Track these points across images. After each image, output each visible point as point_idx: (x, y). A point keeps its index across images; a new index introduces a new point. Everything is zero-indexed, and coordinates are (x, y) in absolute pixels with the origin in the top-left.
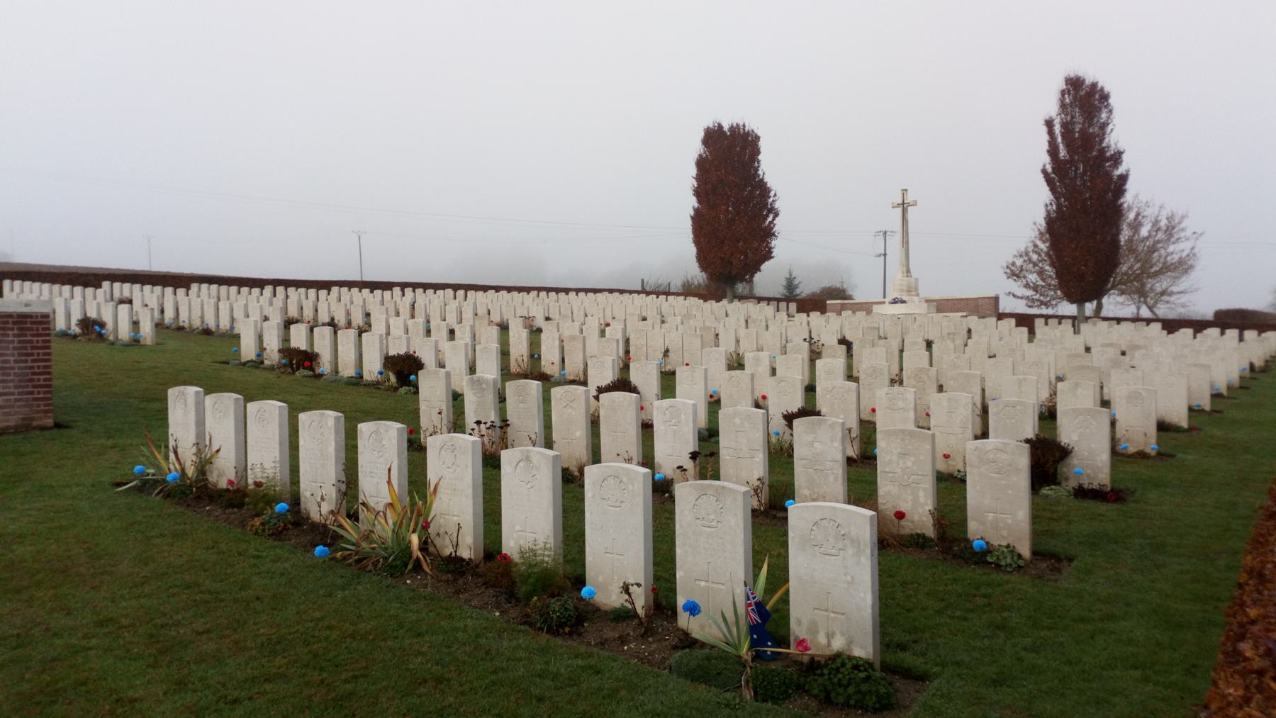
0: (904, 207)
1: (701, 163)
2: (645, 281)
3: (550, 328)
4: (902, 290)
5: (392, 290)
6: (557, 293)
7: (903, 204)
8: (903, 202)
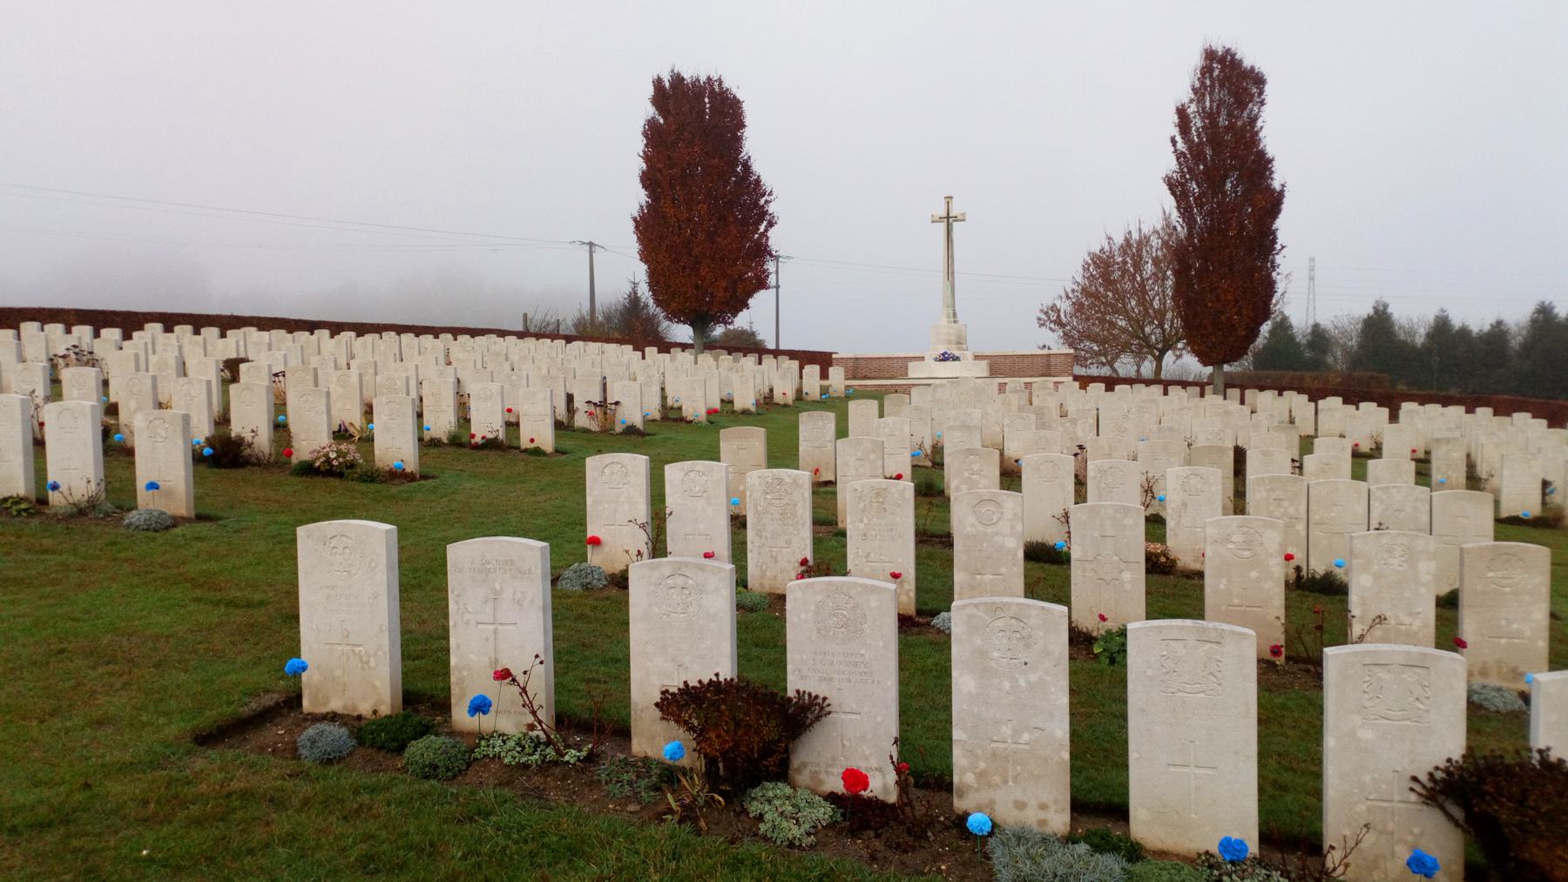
0: (949, 219)
1: (653, 133)
2: (530, 316)
3: (976, 467)
4: (950, 342)
5: (17, 328)
6: (775, 357)
7: (948, 217)
8: (948, 214)
